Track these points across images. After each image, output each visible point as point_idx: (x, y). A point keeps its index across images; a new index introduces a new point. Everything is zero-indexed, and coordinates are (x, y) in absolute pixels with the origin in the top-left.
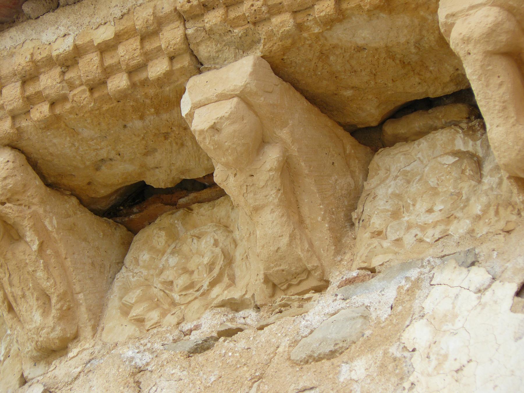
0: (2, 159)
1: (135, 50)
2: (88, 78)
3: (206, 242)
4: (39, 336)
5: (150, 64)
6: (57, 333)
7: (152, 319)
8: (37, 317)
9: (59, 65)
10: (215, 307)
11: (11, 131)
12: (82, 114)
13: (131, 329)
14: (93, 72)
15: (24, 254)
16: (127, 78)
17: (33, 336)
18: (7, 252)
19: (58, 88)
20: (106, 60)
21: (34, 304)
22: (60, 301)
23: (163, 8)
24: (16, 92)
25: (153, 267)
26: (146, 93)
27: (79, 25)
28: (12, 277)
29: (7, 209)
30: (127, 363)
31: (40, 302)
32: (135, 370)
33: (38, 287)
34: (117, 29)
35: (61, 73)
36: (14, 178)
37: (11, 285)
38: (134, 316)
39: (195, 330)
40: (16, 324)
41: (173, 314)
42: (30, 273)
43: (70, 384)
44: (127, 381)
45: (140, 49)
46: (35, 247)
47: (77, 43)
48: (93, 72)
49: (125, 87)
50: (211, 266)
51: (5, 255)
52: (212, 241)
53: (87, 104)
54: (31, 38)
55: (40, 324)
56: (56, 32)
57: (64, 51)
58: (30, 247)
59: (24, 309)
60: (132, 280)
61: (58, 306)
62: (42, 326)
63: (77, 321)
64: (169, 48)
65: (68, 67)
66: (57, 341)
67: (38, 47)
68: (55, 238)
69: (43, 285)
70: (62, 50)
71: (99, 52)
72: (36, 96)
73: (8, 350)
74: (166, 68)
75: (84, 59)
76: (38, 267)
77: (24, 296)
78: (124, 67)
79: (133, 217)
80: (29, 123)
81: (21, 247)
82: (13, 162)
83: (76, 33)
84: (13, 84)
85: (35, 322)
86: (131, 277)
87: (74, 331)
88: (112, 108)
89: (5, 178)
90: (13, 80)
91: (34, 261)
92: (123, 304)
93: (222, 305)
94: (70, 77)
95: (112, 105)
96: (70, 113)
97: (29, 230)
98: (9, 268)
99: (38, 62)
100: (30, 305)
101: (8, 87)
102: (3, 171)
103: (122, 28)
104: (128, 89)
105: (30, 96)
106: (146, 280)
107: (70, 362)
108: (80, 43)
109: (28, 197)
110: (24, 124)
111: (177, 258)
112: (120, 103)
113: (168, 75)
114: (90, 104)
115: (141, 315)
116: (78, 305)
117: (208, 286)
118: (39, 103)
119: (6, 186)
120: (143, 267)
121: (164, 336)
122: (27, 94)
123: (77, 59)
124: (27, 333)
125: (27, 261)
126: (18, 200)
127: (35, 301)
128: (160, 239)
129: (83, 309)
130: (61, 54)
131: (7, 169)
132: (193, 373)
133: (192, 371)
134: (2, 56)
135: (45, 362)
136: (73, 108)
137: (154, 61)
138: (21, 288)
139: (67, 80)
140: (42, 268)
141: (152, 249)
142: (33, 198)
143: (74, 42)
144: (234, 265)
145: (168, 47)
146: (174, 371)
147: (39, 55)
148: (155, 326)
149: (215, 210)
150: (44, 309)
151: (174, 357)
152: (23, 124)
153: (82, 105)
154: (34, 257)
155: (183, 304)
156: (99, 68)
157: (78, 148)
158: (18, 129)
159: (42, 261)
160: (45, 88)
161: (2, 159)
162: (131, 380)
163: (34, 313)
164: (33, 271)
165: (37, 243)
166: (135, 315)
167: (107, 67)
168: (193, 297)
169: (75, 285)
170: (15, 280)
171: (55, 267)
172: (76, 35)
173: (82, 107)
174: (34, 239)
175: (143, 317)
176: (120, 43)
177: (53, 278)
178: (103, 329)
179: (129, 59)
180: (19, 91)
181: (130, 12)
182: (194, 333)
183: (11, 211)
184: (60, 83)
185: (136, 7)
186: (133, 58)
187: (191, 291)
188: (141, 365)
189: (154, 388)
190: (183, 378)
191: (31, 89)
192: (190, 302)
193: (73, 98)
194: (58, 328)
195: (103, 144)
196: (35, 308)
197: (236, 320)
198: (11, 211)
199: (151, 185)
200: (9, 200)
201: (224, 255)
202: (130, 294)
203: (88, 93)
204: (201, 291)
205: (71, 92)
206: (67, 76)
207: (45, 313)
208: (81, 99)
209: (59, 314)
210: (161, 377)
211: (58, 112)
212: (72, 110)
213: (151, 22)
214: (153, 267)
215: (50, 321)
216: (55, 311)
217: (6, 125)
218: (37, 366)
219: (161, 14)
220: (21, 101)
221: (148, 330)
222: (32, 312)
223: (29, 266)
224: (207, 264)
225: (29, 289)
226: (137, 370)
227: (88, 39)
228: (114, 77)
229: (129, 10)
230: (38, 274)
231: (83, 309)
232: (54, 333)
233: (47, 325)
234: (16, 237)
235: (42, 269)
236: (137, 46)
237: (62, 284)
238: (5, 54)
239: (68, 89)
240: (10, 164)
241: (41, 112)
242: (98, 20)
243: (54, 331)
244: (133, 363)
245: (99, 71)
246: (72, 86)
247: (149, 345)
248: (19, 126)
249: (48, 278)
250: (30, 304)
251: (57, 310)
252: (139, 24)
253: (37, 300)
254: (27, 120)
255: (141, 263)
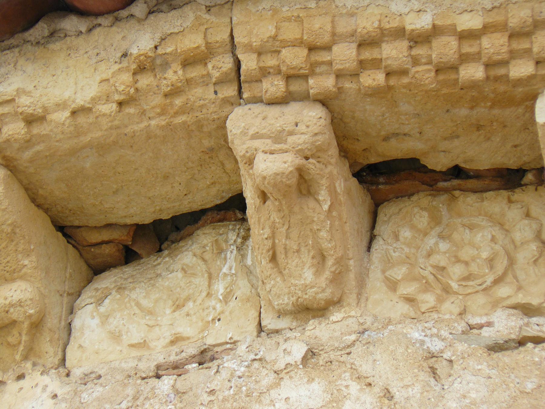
0: (314, 114)
1: (502, 46)
2: (441, 60)
3: (483, 236)
4: (304, 293)
5: (513, 62)
6: (327, 294)
7: (427, 302)
8: (308, 275)
9: (408, 39)
10: (507, 307)
11: (334, 90)
12: (416, 91)
13: (404, 308)
14: (448, 56)
15: (314, 211)
16: (484, 70)
17: (297, 291)
18: (295, 205)
19: (403, 61)
20: (464, 47)
21: (307, 261)
22: (335, 264)
23: (541, 12)
24: (351, 53)
25: (413, 245)
26: (495, 89)
27: (437, 4)
28: (290, 230)
29: (310, 165)
30: (418, 345)
31: (315, 260)
32: (428, 354)
33: (317, 246)
34: (486, 21)
35: (409, 47)
36: (324, 135)
37: (287, 237)
38: (404, 294)
39: (487, 326)
40: (276, 275)
41: (452, 303)
42: (313, 231)
43: (340, 350)
44: (421, 364)
45: (508, 46)
46: (326, 207)
47: (436, 22)
48: (448, 56)
49: (481, 79)
50: (491, 262)
51: (292, 208)
52: (490, 236)
53: (429, 84)
54: (377, 4)
55: (311, 282)
56: (408, 5)
57: (421, 28)
58: (321, 206)
59: (294, 264)
60: (394, 254)
61: (333, 269)
62: (312, 284)
63: (343, 286)
64: (541, 53)
65: (416, 42)
66: (323, 302)
67: (386, 15)
68: (341, 201)
69: (323, 245)
70: (420, 27)
71: (457, 38)
72: (371, 62)
73: (228, 290)
74: (532, 71)
75: (439, 40)
76: (324, 227)
77: (298, 251)
78: (484, 59)
79: (382, 187)
80: (354, 86)
81: (311, 203)
82: (325, 120)
83: (434, 12)
84: (347, 44)
85: (305, 279)
86: (392, 251)
87: (339, 296)
88: (452, 93)
89: (316, 134)
90: (348, 40)
91: (322, 221)
92: (386, 277)
93: (515, 307)
94: (418, 53)
95: (453, 91)
96: (404, 87)
97: (325, 189)
98: (291, 221)
99: (385, 30)
100: (303, 262)
101: (340, 45)
102: (315, 127)
103: (491, 21)
104: (482, 81)
105: (365, 60)
106: (408, 257)
107: (333, 326)
108: (440, 23)
109: (328, 156)
110: (347, 85)
111: (449, 245)
112: (462, 91)
113: (531, 77)
114: (432, 85)
115: (412, 295)
116: (348, 270)
117: (492, 283)
118: (371, 69)
119: (315, 142)
120: (404, 244)
121: (452, 325)
122: (362, 57)
123: (430, 38)
124: (290, 287)
125: (315, 219)
126: (319, 157)
127: (310, 259)
128: (422, 219)
129: (352, 275)
130: (417, 30)
131: (320, 126)
132: (503, 374)
133: (502, 371)
134: (340, 12)
135: (292, 317)
136: (410, 83)
137: (516, 61)
138: (298, 242)
139: (413, 56)
140: (328, 229)
141: (413, 227)
142: (331, 158)
143: (433, 21)
144: (515, 267)
145: (540, 52)
146: (479, 367)
147: (387, 23)
148: (431, 310)
149: (485, 203)
150: (317, 269)
151: (474, 351)
152: (347, 85)
153: (422, 83)
154: (324, 217)
155: (461, 295)
156: (457, 52)
157: (386, 119)
158: (339, 89)
159: (329, 222)
160: (388, 58)
161: (314, 114)
162: (425, 365)
163: (305, 270)
164: (317, 230)
165: (329, 203)
166: (406, 293)
167: (463, 54)
168: (475, 290)
169: (349, 250)
170: (294, 234)
171: (337, 230)
172: (435, 14)
173: (421, 85)
174: (327, 199)
175: (414, 297)
176: (484, 34)
177: (335, 241)
178: (367, 300)
179: (493, 53)
180: (354, 54)
181: (502, 6)
182: (485, 329)
183: (313, 167)
184: (406, 57)
185: (509, 4)
186: (498, 54)
187: (471, 283)
188: (434, 351)
189: (458, 379)
190: (494, 377)
191: (368, 54)
192: (469, 294)
193: (415, 74)
194: (329, 291)
195: (412, 120)
196: (308, 265)
197: (530, 325)
198: (313, 167)
199: (427, 165)
200: (313, 156)
201: (507, 256)
202: (395, 269)
203: (433, 74)
204: (484, 286)
205: (413, 68)
206: (414, 52)
207: (318, 273)
208: (424, 77)
209: (331, 277)
210: (465, 370)
211: (392, 84)
212: (408, 86)
213: (528, 23)
214: (413, 245)
215: (323, 281)
216: (329, 273)
217: (328, 82)
218: (281, 318)
219: (538, 18)
220: (355, 63)
221: (423, 313)
222: (302, 269)
223: (315, 224)
224: (486, 259)
225: (307, 246)
226: (430, 355)
227: (449, 22)
228: (467, 65)
229: (501, 5)
230: (322, 233)
231: (352, 275)
232: (323, 294)
233: (317, 285)
234: (304, 192)
235: (327, 230)
236: (504, 42)
237: (341, 248)
238: (344, 11)
239: (411, 64)
240: (322, 120)
241: (374, 79)
242: (462, 5)
243: (324, 292)
244: (425, 347)
245: (456, 56)
246: (416, 61)
247: (435, 331)
248: (342, 86)
249: (331, 240)
250: (304, 260)
251: (331, 272)
252: (513, 23)
253: (313, 258)
254: (352, 82)
255: (401, 239)
